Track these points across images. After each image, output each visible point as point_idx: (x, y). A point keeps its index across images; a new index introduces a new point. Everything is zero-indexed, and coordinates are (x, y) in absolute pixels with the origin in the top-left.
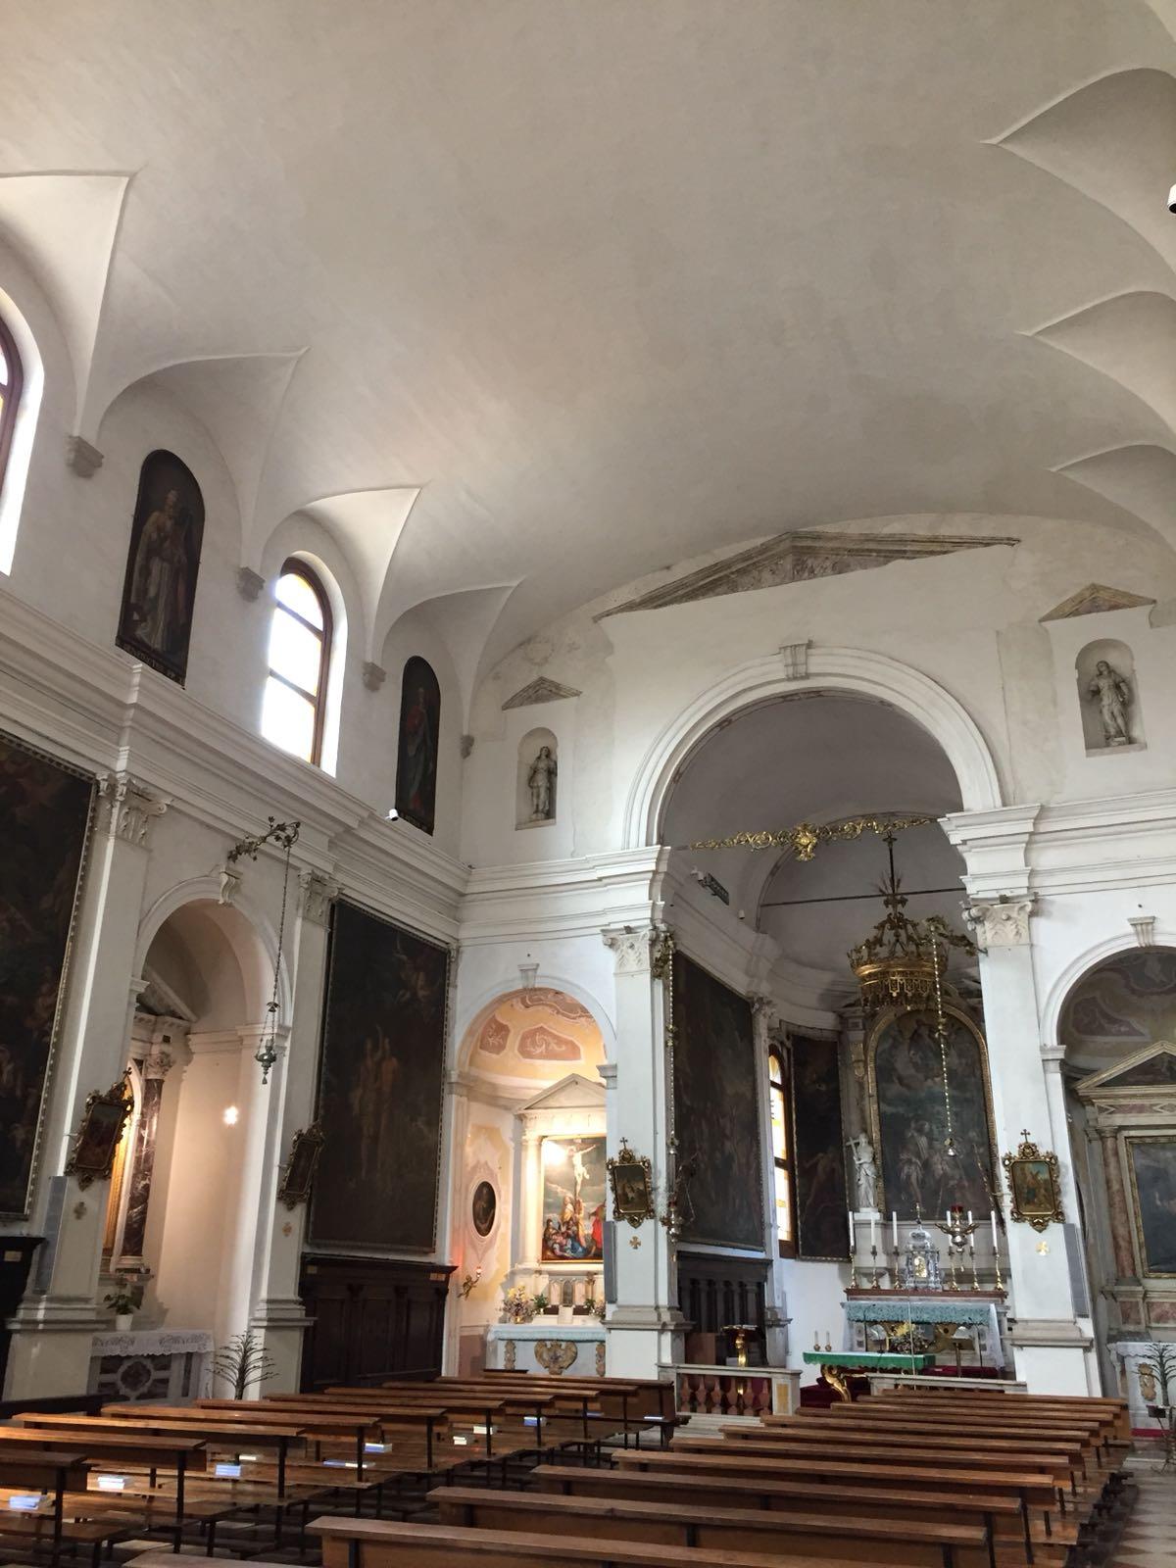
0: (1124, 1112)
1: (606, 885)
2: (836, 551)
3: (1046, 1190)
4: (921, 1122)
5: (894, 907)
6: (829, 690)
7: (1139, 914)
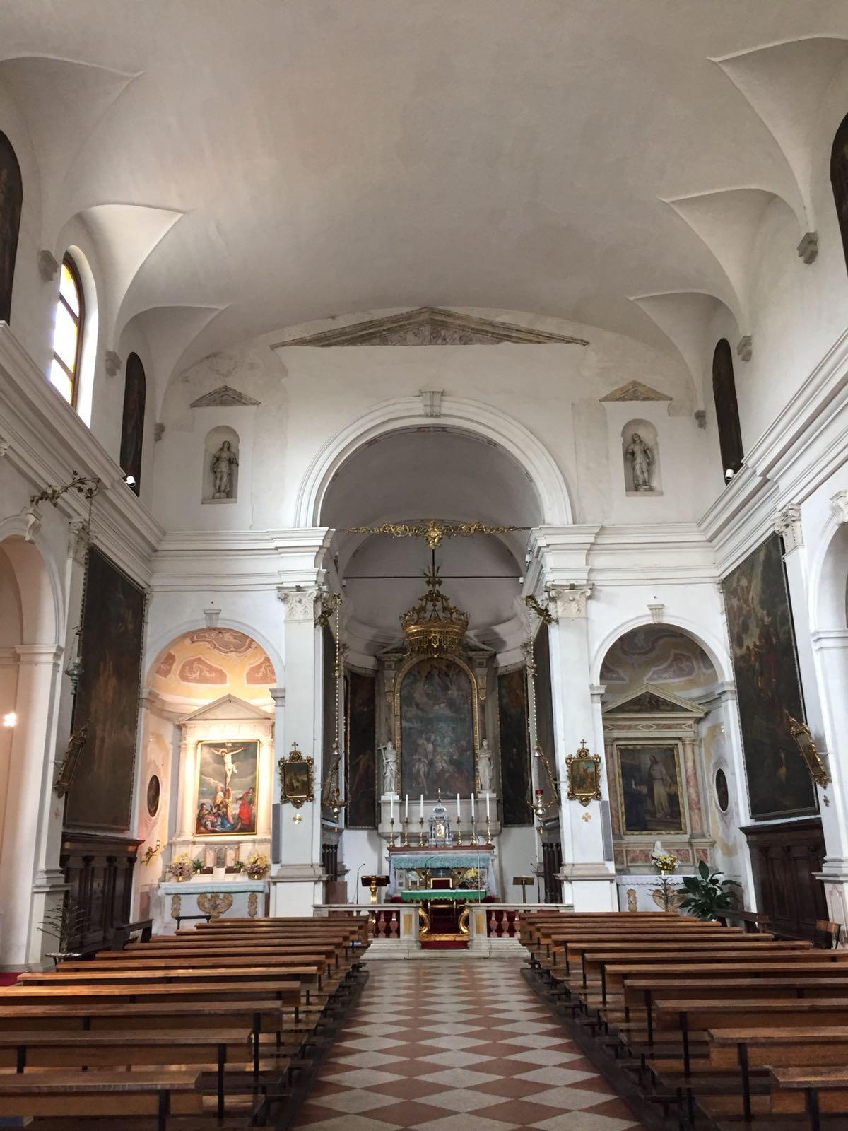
0: (619, 729)
1: (280, 553)
2: (463, 328)
3: (592, 779)
4: (429, 734)
5: (434, 586)
6: (453, 427)
7: (654, 602)
